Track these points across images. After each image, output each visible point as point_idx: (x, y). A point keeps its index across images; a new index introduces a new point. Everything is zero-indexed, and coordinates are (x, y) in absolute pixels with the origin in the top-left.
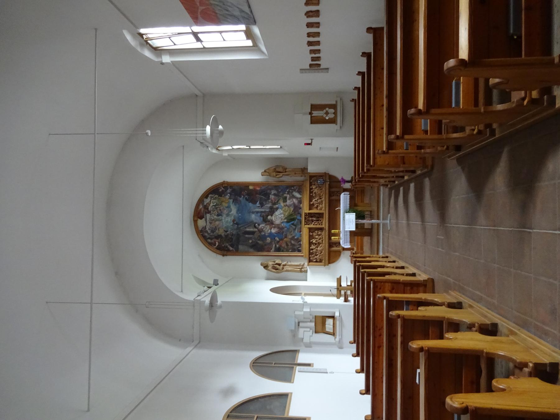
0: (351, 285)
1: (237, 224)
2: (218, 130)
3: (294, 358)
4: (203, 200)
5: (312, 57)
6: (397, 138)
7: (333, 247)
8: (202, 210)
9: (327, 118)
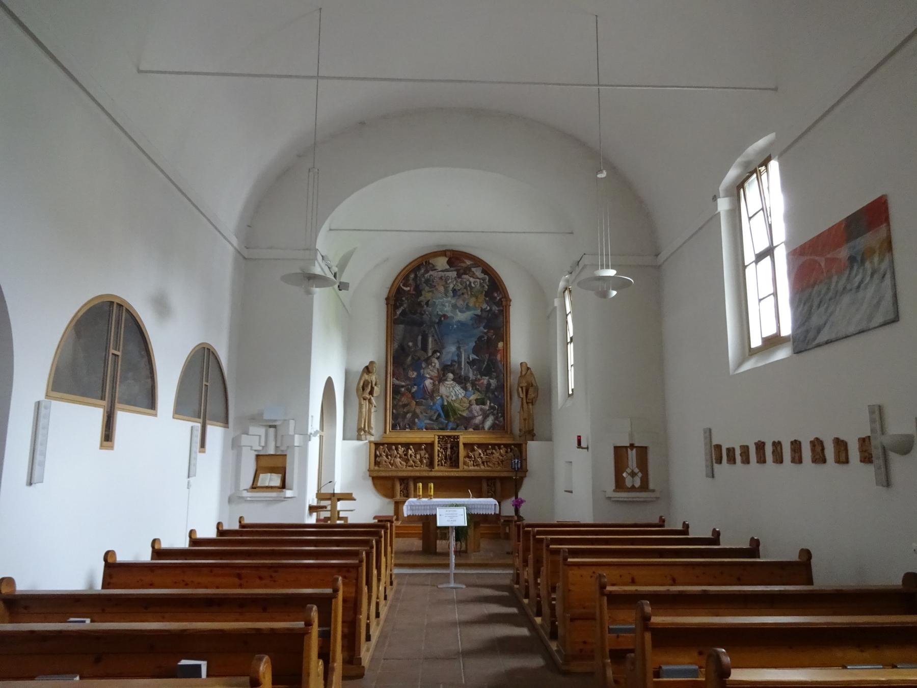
0: (339, 518)
1: (440, 322)
2: (610, 289)
3: (215, 420)
4: (479, 266)
5: (734, 449)
6: (646, 618)
7: (401, 485)
8: (463, 265)
9: (624, 475)
